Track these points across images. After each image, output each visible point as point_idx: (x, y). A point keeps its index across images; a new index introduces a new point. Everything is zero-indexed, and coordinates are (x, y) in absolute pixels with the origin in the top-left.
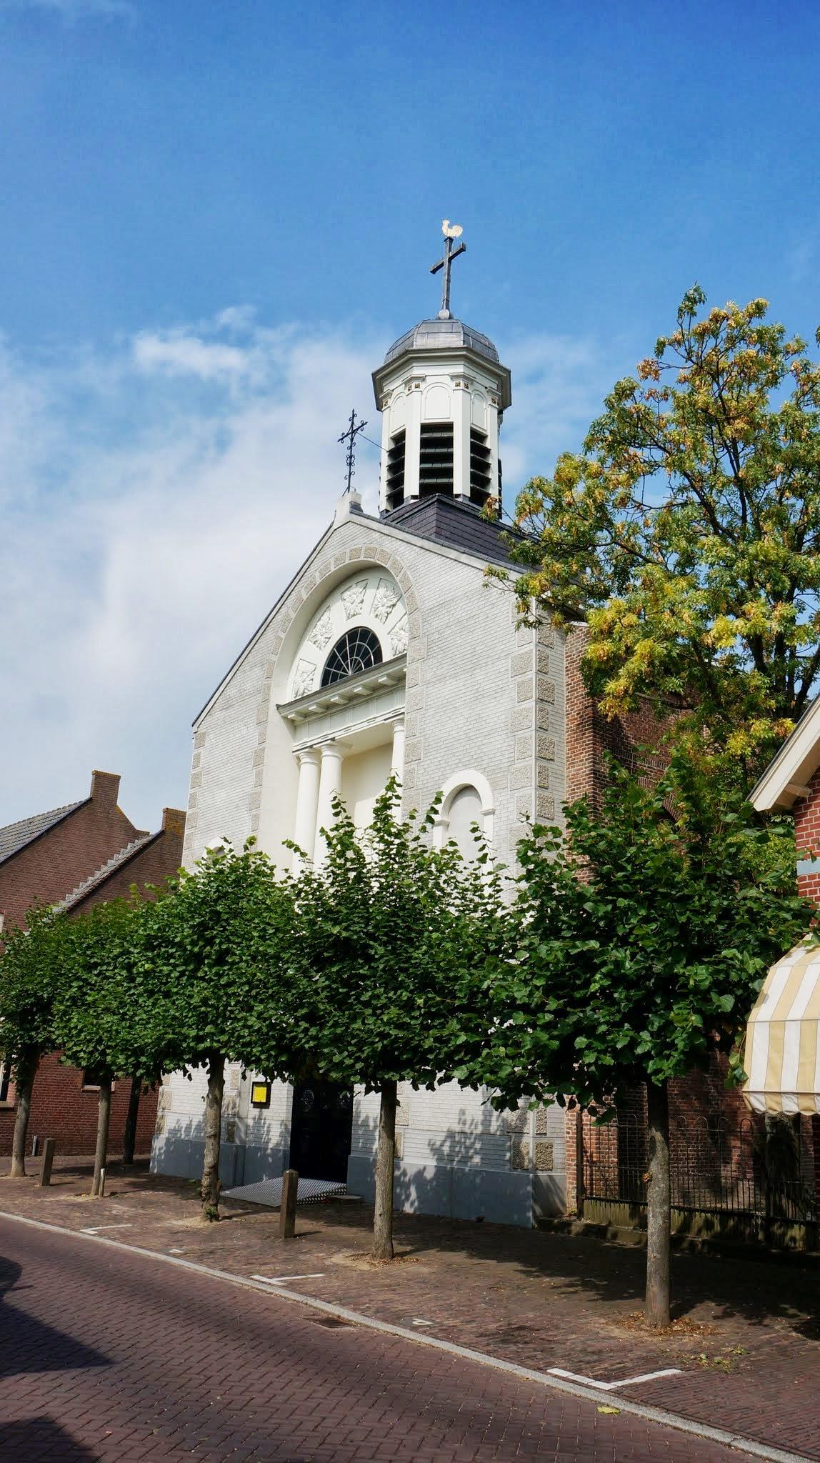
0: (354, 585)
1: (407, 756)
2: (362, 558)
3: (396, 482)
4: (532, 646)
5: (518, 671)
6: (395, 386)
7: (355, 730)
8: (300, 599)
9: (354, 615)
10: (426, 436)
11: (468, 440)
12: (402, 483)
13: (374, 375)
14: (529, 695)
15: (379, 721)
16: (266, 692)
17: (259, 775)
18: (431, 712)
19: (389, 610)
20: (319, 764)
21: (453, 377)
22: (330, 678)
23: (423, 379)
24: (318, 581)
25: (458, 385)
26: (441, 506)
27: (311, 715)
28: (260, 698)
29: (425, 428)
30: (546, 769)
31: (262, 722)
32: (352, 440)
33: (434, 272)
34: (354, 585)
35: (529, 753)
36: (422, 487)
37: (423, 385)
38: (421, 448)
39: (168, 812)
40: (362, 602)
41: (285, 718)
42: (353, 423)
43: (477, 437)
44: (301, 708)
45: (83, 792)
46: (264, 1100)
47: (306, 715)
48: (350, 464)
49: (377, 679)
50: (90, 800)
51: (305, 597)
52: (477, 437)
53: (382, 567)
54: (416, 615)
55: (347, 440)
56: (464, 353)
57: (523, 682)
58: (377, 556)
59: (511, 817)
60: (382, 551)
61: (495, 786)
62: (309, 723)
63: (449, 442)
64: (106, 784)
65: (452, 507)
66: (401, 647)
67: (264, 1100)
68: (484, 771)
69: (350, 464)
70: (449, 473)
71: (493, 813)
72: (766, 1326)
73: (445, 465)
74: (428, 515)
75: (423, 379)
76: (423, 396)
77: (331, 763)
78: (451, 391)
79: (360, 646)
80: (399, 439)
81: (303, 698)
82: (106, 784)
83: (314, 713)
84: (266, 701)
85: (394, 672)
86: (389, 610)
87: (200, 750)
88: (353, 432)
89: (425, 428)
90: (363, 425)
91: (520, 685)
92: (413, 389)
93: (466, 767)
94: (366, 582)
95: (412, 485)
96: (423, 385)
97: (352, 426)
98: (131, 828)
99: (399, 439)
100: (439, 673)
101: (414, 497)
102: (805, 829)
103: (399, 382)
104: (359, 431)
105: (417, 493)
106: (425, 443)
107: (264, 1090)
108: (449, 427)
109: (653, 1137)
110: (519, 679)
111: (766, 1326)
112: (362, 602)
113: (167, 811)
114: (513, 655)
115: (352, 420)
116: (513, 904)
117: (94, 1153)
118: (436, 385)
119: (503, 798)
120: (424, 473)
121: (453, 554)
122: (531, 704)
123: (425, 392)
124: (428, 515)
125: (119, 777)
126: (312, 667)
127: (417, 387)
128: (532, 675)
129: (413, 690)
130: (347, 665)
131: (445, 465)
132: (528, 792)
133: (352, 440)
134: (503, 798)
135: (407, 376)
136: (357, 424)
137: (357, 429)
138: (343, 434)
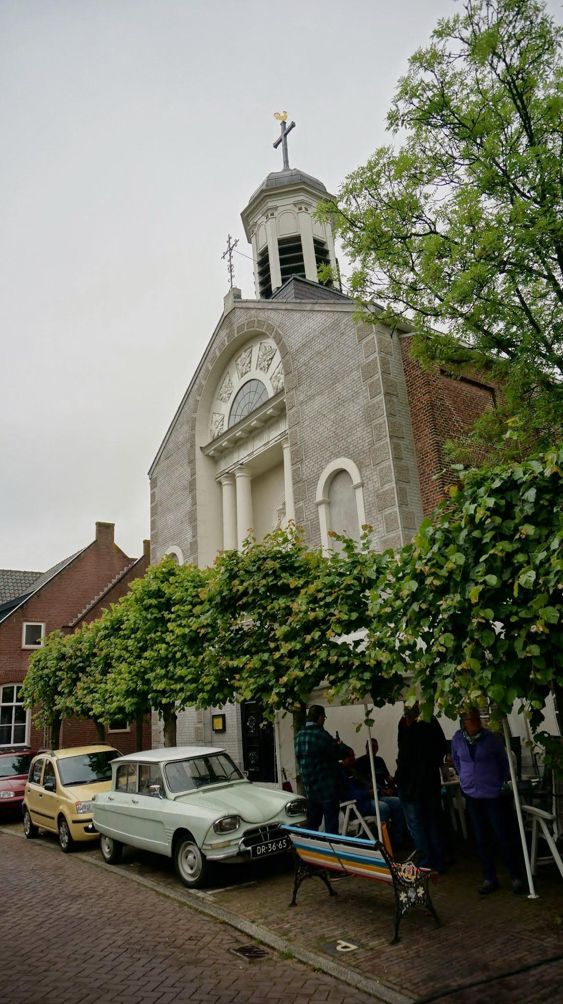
1: (292, 459)
2: (246, 330)
4: (376, 355)
5: (368, 371)
6: (260, 219)
8: (207, 370)
9: (246, 373)
12: (268, 261)
13: (242, 214)
14: (379, 391)
15: (272, 444)
16: (192, 440)
17: (194, 498)
18: (307, 423)
20: (234, 484)
21: (295, 204)
23: (276, 208)
24: (218, 354)
25: (300, 209)
26: (297, 283)
28: (189, 445)
30: (399, 445)
31: (192, 462)
33: (337, 732)
34: (243, 353)
35: (384, 434)
38: (280, 255)
41: (208, 456)
45: (90, 537)
46: (221, 728)
49: (266, 412)
51: (210, 368)
54: (287, 357)
57: (373, 383)
58: (256, 325)
59: (376, 486)
60: (259, 321)
61: (360, 466)
63: (299, 248)
64: (105, 530)
65: (306, 283)
66: (280, 386)
67: (221, 728)
74: (288, 291)
75: (276, 208)
76: (277, 221)
77: (242, 483)
78: (295, 214)
82: (105, 530)
84: (193, 446)
87: (155, 490)
89: (281, 242)
91: (371, 386)
92: (270, 217)
93: (337, 457)
95: (276, 280)
96: (276, 214)
97: (229, 246)
98: (125, 557)
100: (309, 393)
106: (282, 251)
107: (220, 720)
108: (298, 238)
109: (436, 684)
110: (370, 381)
114: (362, 365)
115: (229, 242)
118: (285, 212)
119: (369, 473)
121: (309, 307)
122: (382, 397)
124: (288, 291)
125: (112, 525)
126: (222, 416)
127: (272, 215)
128: (379, 376)
129: (291, 411)
132: (388, 463)
134: (369, 473)
135: (265, 208)
136: (232, 242)
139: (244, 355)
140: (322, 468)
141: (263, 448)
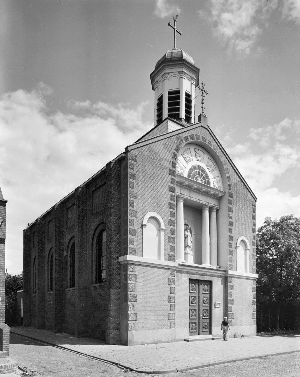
6: (159, 78)
10: (169, 96)
23: (168, 73)
29: (170, 93)
37: (169, 76)
43: (188, 96)
48: (203, 103)
52: (188, 96)
63: (178, 98)
68: (246, 237)
69: (203, 103)
70: (178, 109)
73: (170, 107)
75: (168, 73)
89: (170, 93)
103: (160, 76)
106: (170, 99)
116: (7, 274)
120: (169, 110)
123: (169, 79)
125: (212, 281)
131: (170, 107)
138: (207, 91)
141: (198, 200)
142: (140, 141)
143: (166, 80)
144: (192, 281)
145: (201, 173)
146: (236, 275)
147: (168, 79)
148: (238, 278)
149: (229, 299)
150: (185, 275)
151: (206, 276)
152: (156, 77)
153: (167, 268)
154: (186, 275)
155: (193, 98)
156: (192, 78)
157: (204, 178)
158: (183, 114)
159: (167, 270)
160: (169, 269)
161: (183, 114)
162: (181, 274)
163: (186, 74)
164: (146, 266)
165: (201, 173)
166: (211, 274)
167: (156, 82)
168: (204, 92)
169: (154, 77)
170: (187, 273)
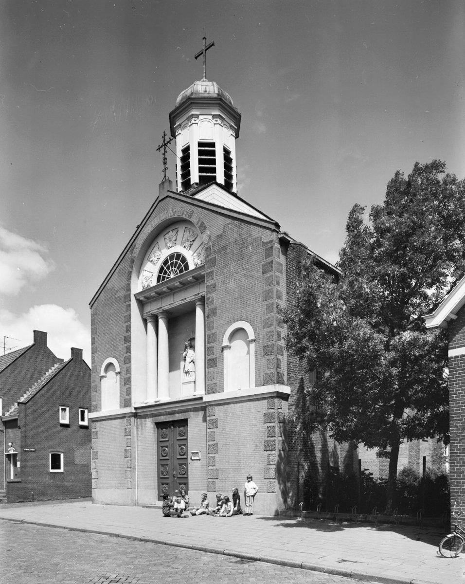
0: (171, 232)
3: (186, 173)
7: (175, 304)
11: (223, 153)
19: (192, 243)
22: (158, 281)
27: (151, 298)
29: (200, 144)
32: (165, 149)
34: (171, 232)
36: (200, 177)
39: (73, 350)
40: (176, 240)
42: (164, 139)
43: (227, 152)
44: (146, 295)
47: (147, 298)
50: (33, 346)
52: (227, 152)
53: (190, 221)
55: (162, 150)
56: (219, 102)
62: (162, 298)
63: (213, 153)
69: (165, 163)
70: (214, 170)
71: (255, 340)
72: (185, 517)
79: (176, 263)
80: (186, 151)
81: (147, 290)
83: (153, 297)
85: (196, 275)
86: (192, 243)
88: (165, 145)
89: (200, 144)
90: (159, 149)
94: (176, 230)
98: (54, 357)
99: (186, 151)
101: (197, 184)
102: (455, 341)
104: (169, 145)
105: (198, 181)
106: (201, 153)
111: (185, 517)
112: (176, 240)
113: (72, 349)
115: (164, 137)
117: (416, 517)
120: (201, 170)
125: (46, 333)
126: (151, 274)
130: (170, 272)
133: (165, 149)
137: (167, 143)
139: (171, 233)
140: (235, 321)
141: (181, 302)
142: (268, 220)
143: (194, 125)
144: (159, 425)
145: (169, 265)
146: (220, 400)
147: (197, 124)
148: (229, 403)
149: (14, 477)
150: (149, 419)
151: (178, 413)
152: (178, 117)
153: (122, 417)
154: (151, 419)
155: (233, 156)
156: (231, 126)
157: (165, 273)
158: (220, 178)
159: (123, 420)
160: (124, 417)
161: (220, 178)
162: (141, 420)
163: (224, 118)
164: (105, 420)
165: (169, 265)
166: (186, 408)
167: (177, 126)
168: (166, 142)
169: (175, 118)
170: (152, 416)
